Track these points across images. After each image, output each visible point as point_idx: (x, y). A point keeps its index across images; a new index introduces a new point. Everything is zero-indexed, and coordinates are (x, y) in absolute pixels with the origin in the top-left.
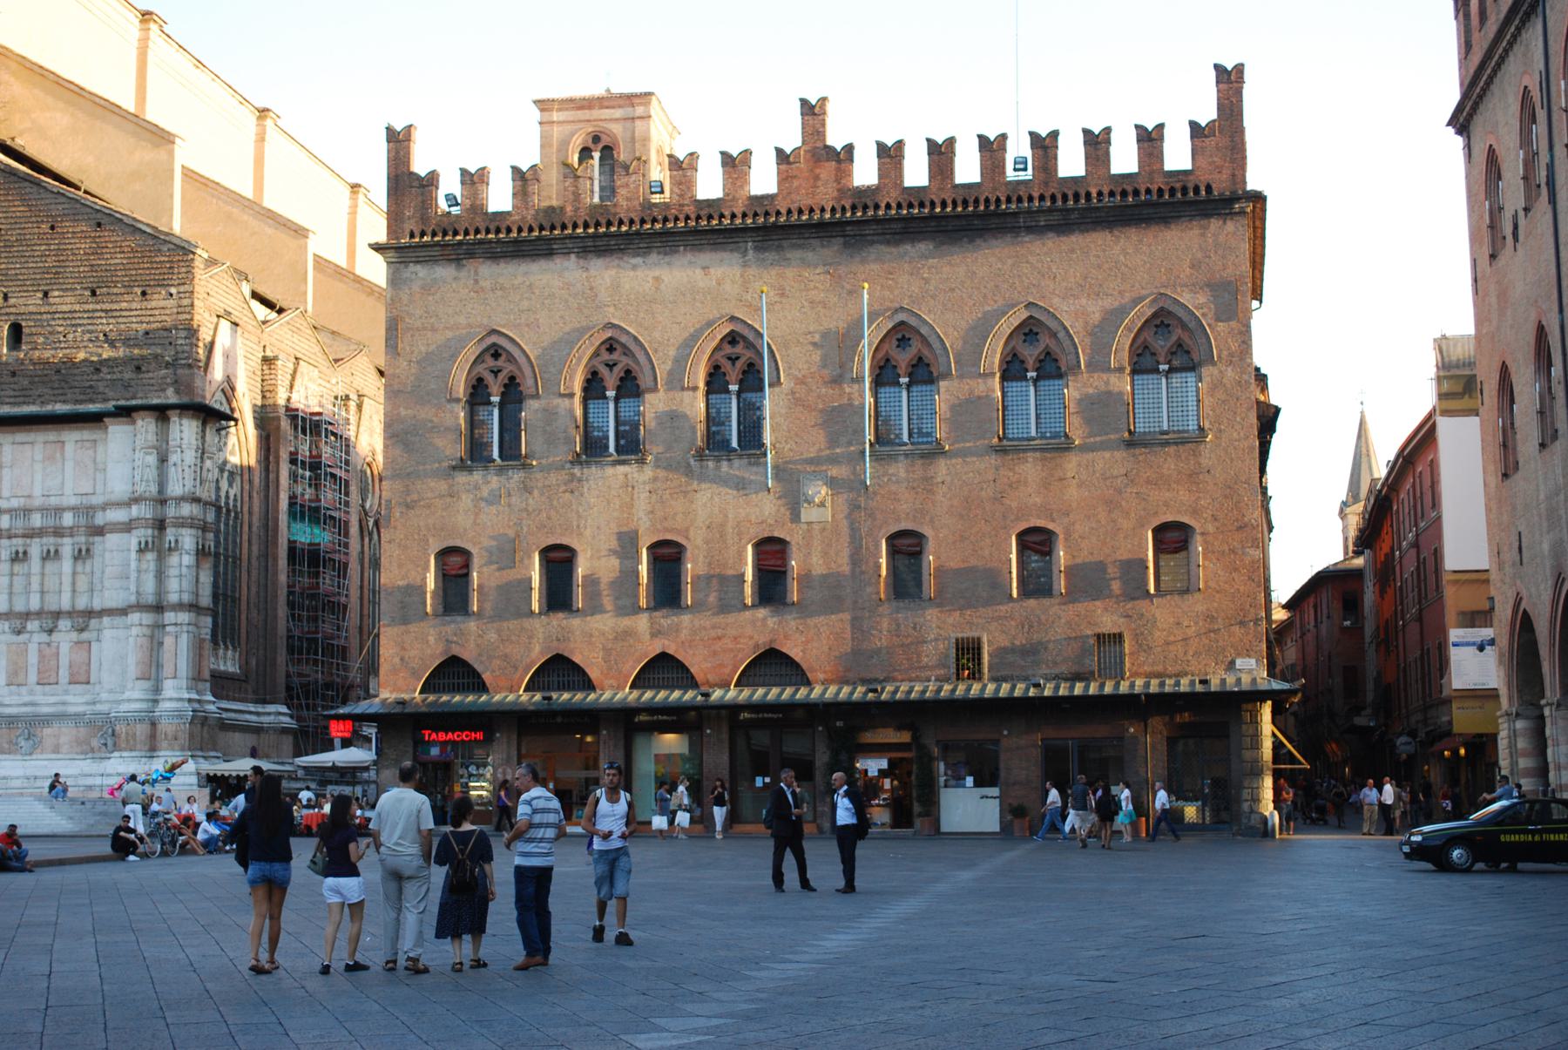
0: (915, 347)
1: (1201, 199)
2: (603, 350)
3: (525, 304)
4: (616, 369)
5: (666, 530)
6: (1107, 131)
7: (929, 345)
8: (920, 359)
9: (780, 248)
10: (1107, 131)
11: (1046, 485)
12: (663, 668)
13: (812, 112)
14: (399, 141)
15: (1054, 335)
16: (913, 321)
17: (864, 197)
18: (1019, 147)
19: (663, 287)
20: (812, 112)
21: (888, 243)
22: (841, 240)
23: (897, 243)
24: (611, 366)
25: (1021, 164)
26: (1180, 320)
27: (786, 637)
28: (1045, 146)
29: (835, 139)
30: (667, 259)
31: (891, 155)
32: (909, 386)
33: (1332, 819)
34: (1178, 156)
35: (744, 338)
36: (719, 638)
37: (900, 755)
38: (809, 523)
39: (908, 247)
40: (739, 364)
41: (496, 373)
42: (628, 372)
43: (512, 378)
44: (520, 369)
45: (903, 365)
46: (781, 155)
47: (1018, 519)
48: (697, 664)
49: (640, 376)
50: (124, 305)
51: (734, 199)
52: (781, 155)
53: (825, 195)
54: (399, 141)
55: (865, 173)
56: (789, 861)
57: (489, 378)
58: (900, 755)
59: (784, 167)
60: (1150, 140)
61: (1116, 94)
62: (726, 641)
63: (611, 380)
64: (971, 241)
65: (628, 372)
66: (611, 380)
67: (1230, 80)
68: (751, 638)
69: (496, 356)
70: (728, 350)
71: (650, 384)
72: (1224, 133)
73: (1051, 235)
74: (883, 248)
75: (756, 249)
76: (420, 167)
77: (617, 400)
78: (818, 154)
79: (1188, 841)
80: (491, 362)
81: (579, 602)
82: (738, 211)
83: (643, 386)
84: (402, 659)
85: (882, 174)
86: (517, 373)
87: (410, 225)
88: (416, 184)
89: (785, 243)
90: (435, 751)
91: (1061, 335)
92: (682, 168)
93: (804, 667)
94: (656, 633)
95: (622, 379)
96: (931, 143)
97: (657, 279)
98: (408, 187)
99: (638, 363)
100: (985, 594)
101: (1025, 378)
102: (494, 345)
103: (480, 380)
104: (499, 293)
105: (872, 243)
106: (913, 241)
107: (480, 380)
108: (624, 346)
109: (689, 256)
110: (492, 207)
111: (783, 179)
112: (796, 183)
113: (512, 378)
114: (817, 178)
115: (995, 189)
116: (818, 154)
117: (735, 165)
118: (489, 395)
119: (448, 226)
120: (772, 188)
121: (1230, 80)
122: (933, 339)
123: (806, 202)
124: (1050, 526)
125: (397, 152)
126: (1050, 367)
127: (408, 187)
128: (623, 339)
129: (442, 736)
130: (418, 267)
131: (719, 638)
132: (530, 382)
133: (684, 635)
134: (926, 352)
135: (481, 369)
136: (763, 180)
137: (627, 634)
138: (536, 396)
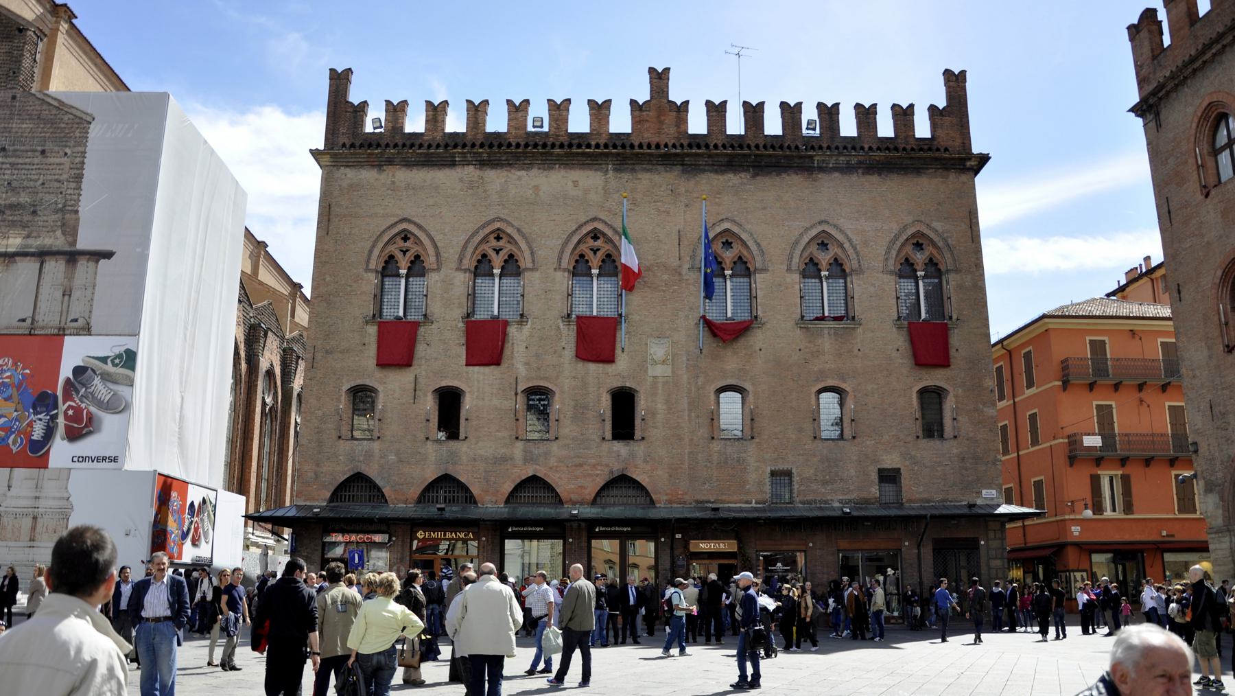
0: (833, 250)
1: (937, 155)
3: (431, 202)
4: (408, 254)
7: (747, 247)
8: (740, 258)
9: (633, 170)
12: (446, 484)
13: (659, 78)
15: (841, 246)
16: (735, 229)
17: (696, 140)
18: (809, 113)
19: (541, 193)
20: (659, 78)
21: (716, 172)
22: (680, 168)
23: (723, 173)
24: (595, 251)
26: (931, 240)
29: (676, 96)
30: (546, 173)
31: (716, 111)
35: (604, 235)
36: (581, 465)
37: (726, 562)
38: (654, 377)
39: (731, 176)
40: (599, 254)
41: (595, 251)
42: (511, 256)
43: (417, 257)
44: (425, 250)
45: (451, 253)
47: (817, 380)
48: (563, 484)
49: (521, 259)
50: (28, 160)
51: (599, 134)
53: (668, 135)
55: (697, 124)
56: (577, 655)
57: (399, 255)
58: (726, 562)
59: (637, 113)
61: (888, 80)
62: (586, 467)
63: (497, 261)
65: (511, 256)
66: (497, 261)
67: (955, 82)
68: (607, 466)
69: (405, 239)
70: (591, 243)
71: (530, 265)
72: (953, 112)
73: (837, 174)
74: (712, 175)
75: (615, 170)
76: (355, 97)
77: (407, 277)
78: (659, 106)
82: (602, 142)
83: (522, 266)
84: (316, 474)
86: (421, 252)
87: (343, 139)
88: (350, 110)
89: (637, 167)
90: (339, 551)
91: (847, 245)
94: (528, 459)
95: (505, 261)
96: (709, 104)
97: (536, 188)
99: (520, 249)
100: (794, 437)
101: (398, 275)
102: (405, 230)
103: (391, 257)
104: (411, 192)
105: (704, 171)
106: (735, 172)
107: (391, 257)
108: (509, 235)
109: (563, 172)
111: (636, 122)
112: (646, 125)
113: (417, 257)
115: (794, 140)
116: (659, 106)
118: (399, 268)
119: (372, 142)
120: (627, 129)
121: (955, 82)
122: (750, 243)
123: (654, 139)
125: (338, 87)
126: (812, 268)
128: (509, 230)
129: (347, 537)
130: (348, 170)
131: (581, 465)
132: (758, 258)
133: (553, 462)
135: (392, 249)
136: (620, 122)
137: (504, 459)
138: (765, 270)
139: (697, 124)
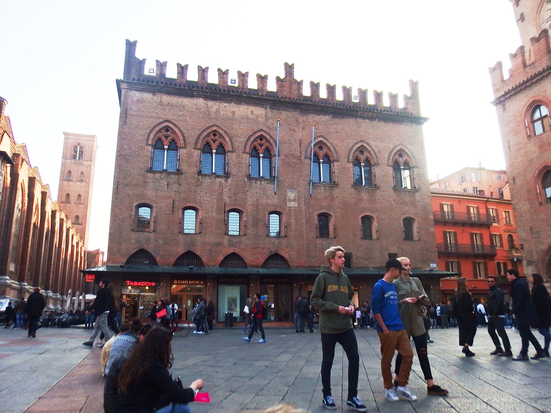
0: (366, 154)
2: (212, 134)
5: (236, 205)
6: (187, 66)
9: (278, 109)
10: (187, 66)
11: (370, 201)
13: (289, 68)
14: (131, 46)
15: (370, 152)
20: (289, 68)
25: (233, 81)
27: (282, 249)
28: (243, 76)
30: (238, 106)
32: (168, 149)
33: (307, 330)
34: (401, 104)
40: (263, 147)
46: (278, 79)
48: (248, 257)
52: (278, 79)
54: (131, 46)
60: (262, 79)
64: (343, 118)
67: (414, 86)
72: (413, 98)
75: (270, 108)
78: (288, 80)
79: (221, 338)
80: (259, 141)
81: (374, 236)
85: (345, 96)
89: (281, 108)
91: (372, 152)
92: (223, 74)
93: (289, 260)
98: (133, 63)
102: (167, 126)
105: (310, 113)
108: (220, 134)
110: (168, 76)
114: (291, 88)
116: (288, 80)
117: (262, 79)
121: (414, 86)
124: (372, 215)
127: (133, 63)
128: (221, 131)
133: (243, 246)
134: (328, 152)
135: (209, 139)
136: (272, 87)
139: (306, 92)
